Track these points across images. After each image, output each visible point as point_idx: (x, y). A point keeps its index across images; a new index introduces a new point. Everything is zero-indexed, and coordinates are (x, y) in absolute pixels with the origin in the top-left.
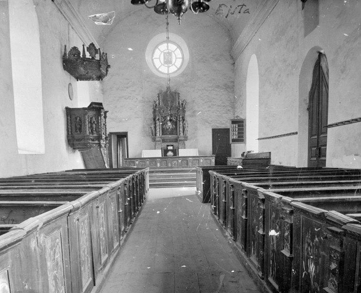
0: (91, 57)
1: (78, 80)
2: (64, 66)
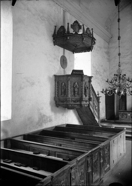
0: (74, 33)
1: (74, 53)
2: (54, 42)
